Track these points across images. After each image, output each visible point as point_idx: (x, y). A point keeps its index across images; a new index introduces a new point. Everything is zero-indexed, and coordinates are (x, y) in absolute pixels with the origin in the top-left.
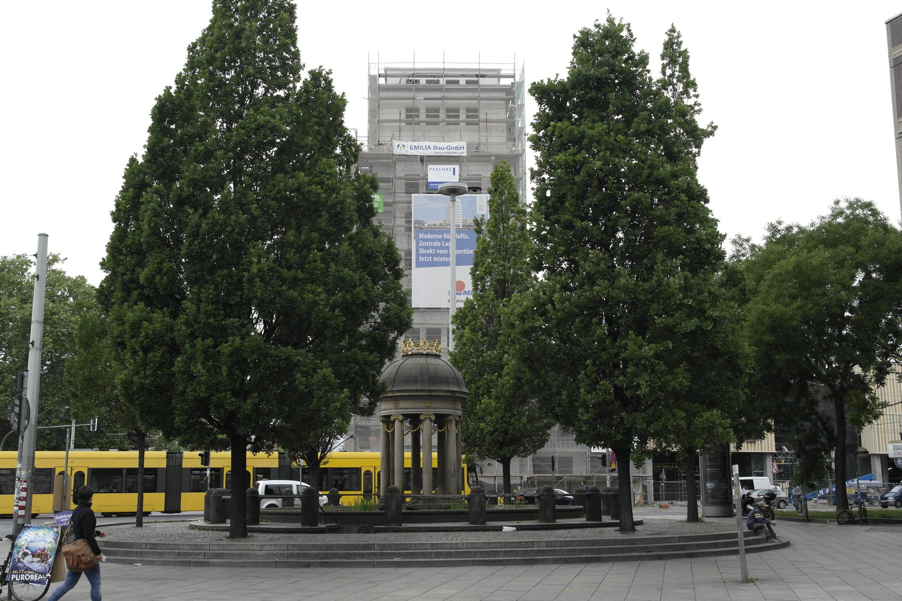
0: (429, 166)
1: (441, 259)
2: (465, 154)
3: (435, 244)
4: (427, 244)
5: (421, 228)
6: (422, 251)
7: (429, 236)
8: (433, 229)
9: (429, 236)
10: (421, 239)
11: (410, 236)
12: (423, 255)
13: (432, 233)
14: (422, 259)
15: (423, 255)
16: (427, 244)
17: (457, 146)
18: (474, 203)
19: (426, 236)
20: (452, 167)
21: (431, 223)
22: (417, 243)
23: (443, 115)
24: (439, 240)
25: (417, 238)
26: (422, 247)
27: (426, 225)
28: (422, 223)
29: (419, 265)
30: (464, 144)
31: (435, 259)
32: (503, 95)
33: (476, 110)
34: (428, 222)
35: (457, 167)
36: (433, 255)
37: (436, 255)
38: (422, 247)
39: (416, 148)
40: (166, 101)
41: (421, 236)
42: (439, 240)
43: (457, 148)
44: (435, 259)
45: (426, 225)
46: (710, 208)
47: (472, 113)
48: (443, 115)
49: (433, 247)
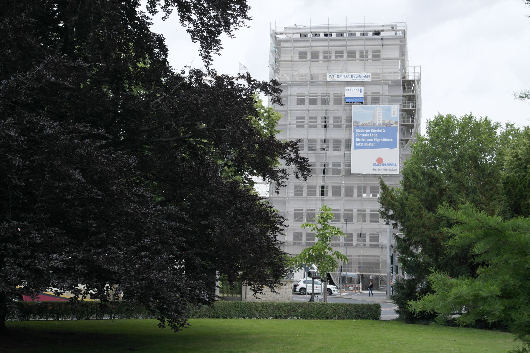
0: (346, 88)
1: (369, 145)
2: (369, 80)
3: (365, 136)
4: (361, 135)
5: (358, 126)
6: (357, 140)
7: (362, 130)
8: (365, 127)
9: (362, 130)
10: (357, 132)
11: (350, 130)
12: (358, 142)
13: (364, 128)
14: (357, 144)
15: (358, 142)
16: (361, 135)
17: (366, 76)
18: (389, 110)
19: (360, 131)
20: (359, 88)
21: (363, 122)
22: (355, 135)
23: (345, 55)
24: (368, 133)
25: (355, 132)
26: (358, 137)
27: (360, 124)
28: (358, 122)
29: (356, 148)
30: (370, 74)
31: (366, 144)
32: (398, 42)
33: (379, 51)
34: (362, 122)
35: (363, 88)
36: (364, 142)
37: (366, 142)
38: (358, 137)
39: (341, 76)
40: (154, 60)
41: (357, 130)
42: (368, 133)
43: (365, 76)
44: (366, 144)
45: (360, 124)
46: (223, 44)
47: (377, 55)
48: (345, 55)
49: (364, 137)
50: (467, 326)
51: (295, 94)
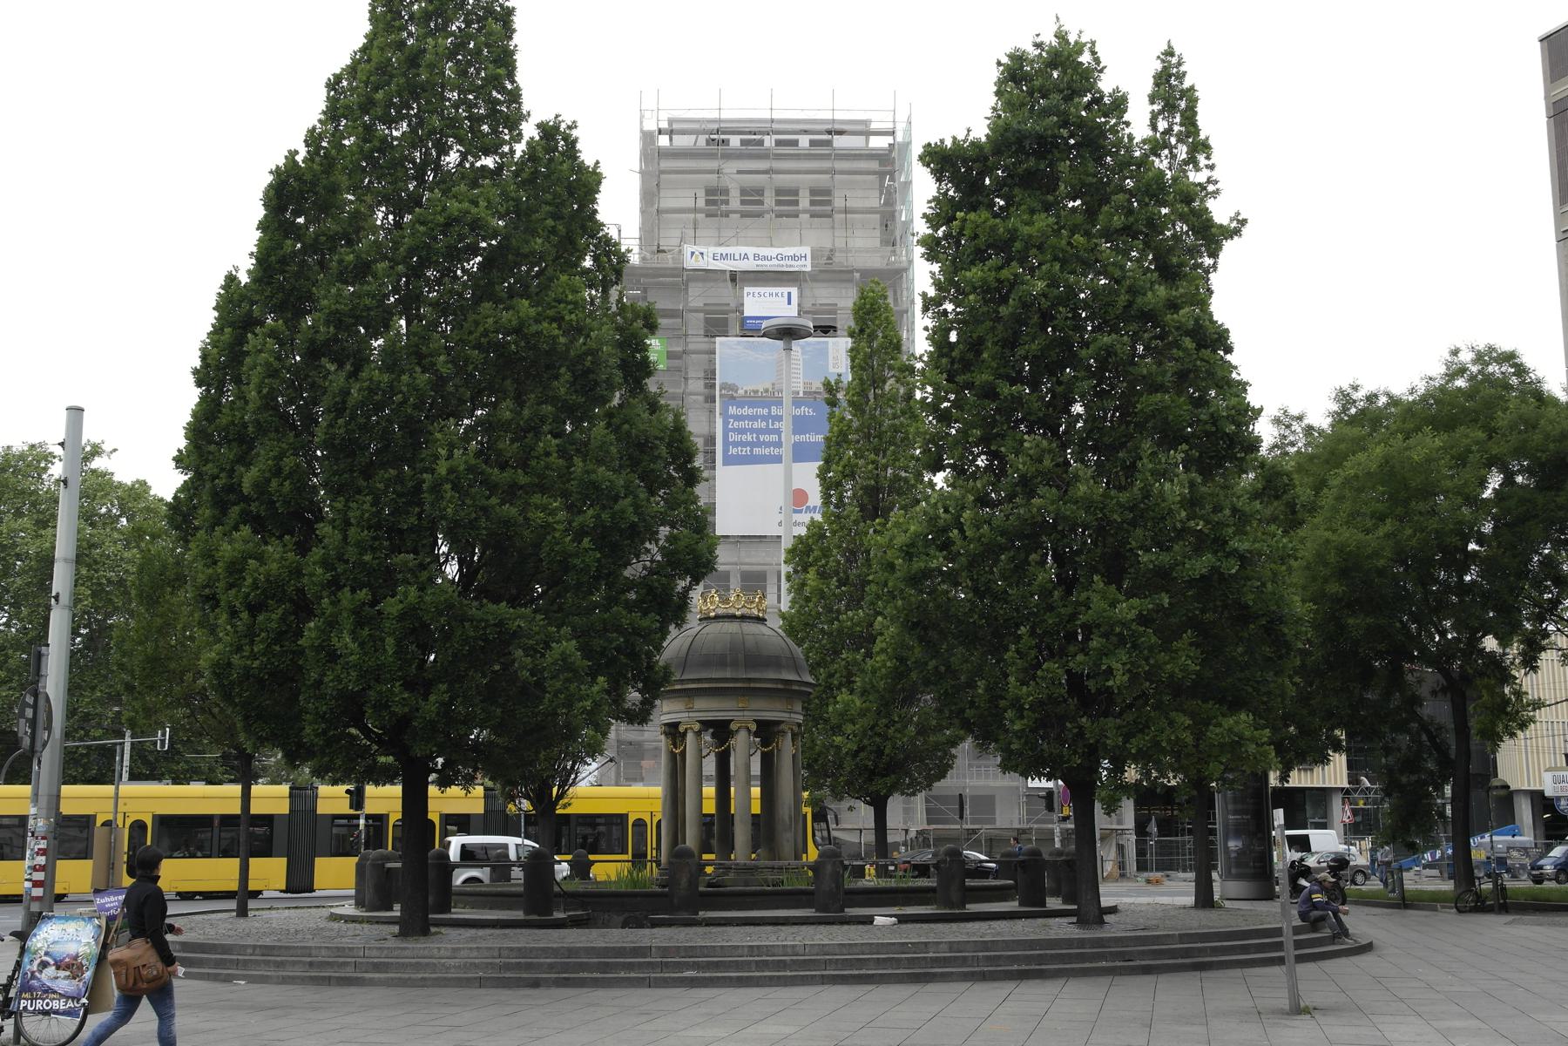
0: (747, 290)
1: (767, 451)
2: (808, 267)
3: (756, 425)
4: (742, 424)
5: (732, 397)
6: (733, 437)
7: (746, 411)
8: (753, 399)
9: (746, 411)
10: (732, 416)
11: (712, 411)
12: (736, 444)
13: (752, 405)
14: (733, 451)
15: (736, 444)
16: (742, 424)
17: (795, 253)
18: (824, 352)
19: (740, 412)
20: (785, 290)
21: (749, 388)
22: (726, 423)
23: (769, 200)
24: (764, 418)
25: (725, 415)
26: (734, 430)
27: (741, 392)
28: (734, 388)
29: (729, 460)
30: (806, 250)
31: (757, 451)
32: (874, 165)
33: (828, 192)
34: (745, 387)
35: (794, 291)
36: (752, 445)
37: (759, 444)
38: (734, 430)
39: (724, 257)
41: (732, 410)
42: (764, 418)
43: (794, 257)
44: (757, 451)
45: (741, 392)
47: (821, 196)
48: (769, 200)
49: (752, 431)
50: (481, 983)
51: (699, 303)
